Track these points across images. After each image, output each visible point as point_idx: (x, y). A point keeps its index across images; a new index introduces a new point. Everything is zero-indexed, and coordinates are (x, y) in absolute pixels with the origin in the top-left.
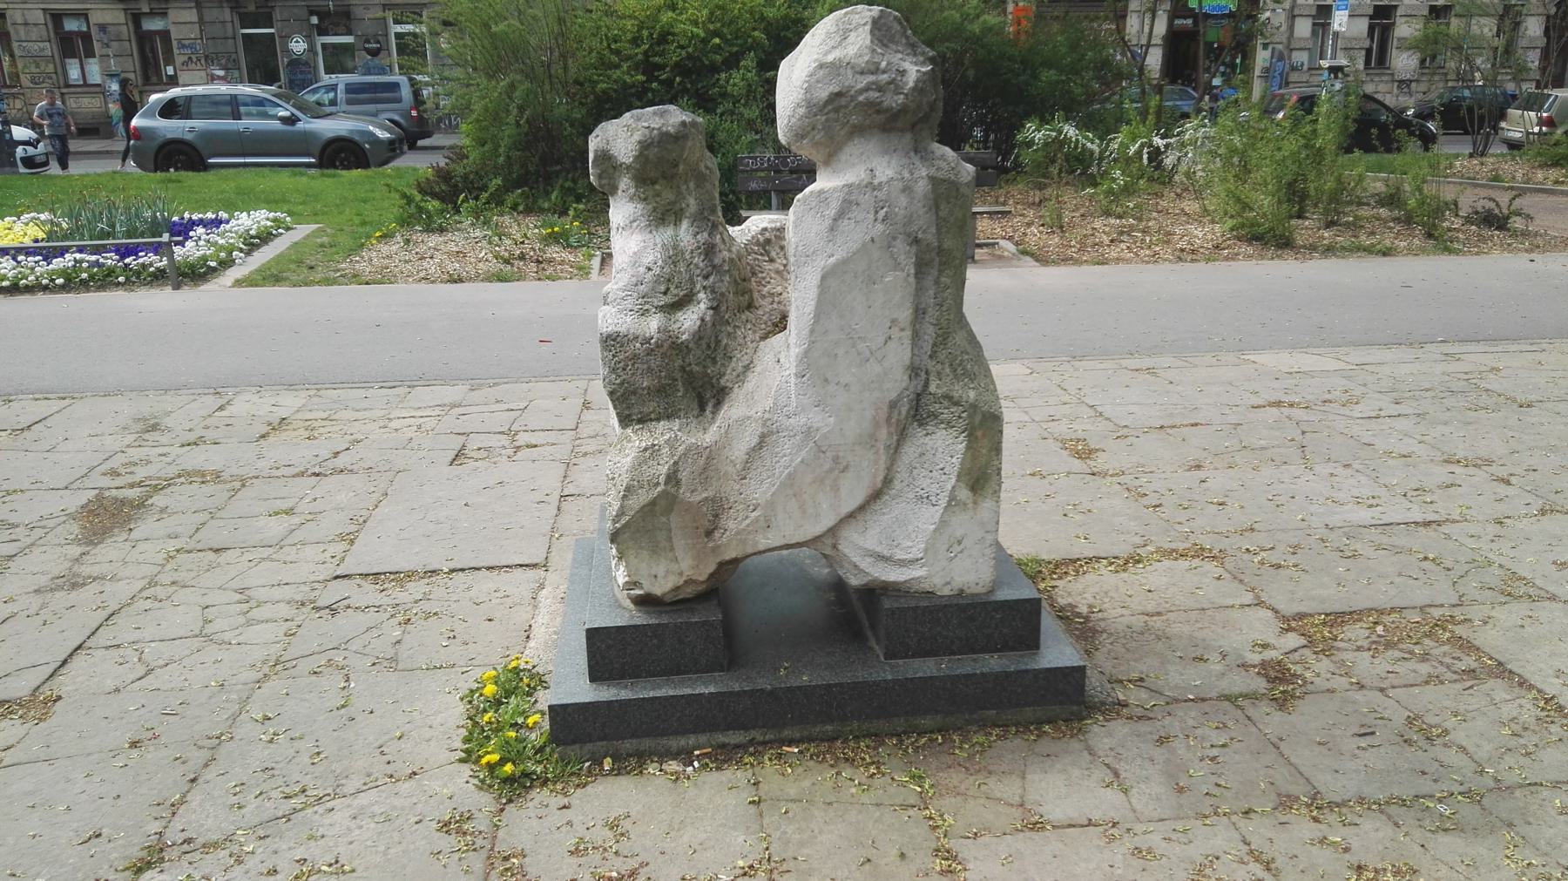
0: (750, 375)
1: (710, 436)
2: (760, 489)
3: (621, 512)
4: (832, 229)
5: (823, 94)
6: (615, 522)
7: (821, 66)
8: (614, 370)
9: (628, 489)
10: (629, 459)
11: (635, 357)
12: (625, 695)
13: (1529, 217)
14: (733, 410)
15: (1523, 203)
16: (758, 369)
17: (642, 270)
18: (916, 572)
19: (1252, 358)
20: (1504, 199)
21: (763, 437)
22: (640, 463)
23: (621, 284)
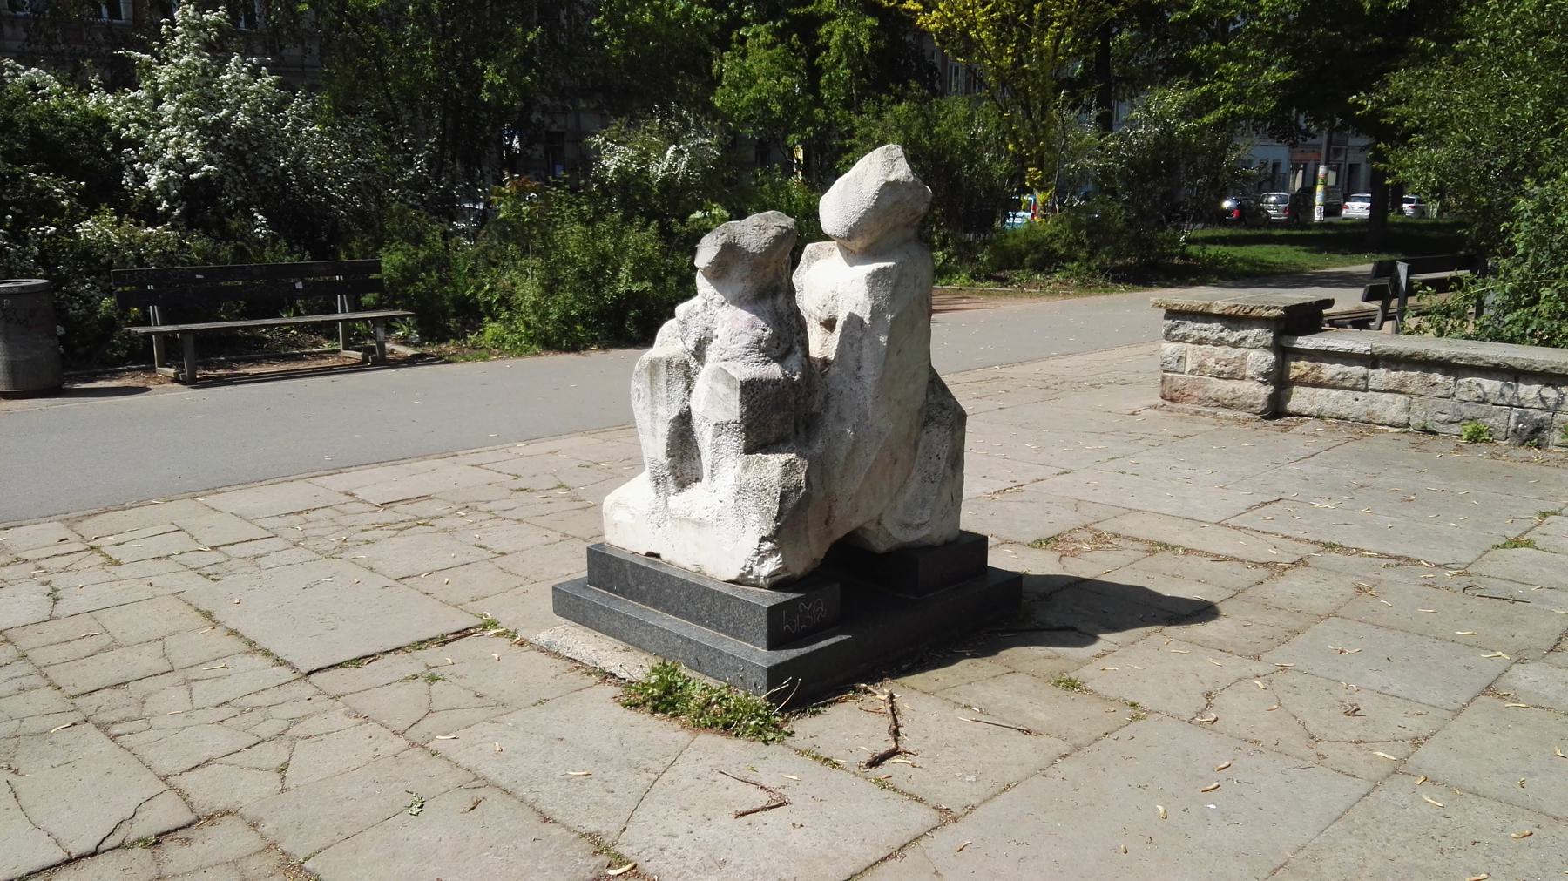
3: (780, 513)
9: (783, 495)
18: (924, 532)
22: (785, 474)
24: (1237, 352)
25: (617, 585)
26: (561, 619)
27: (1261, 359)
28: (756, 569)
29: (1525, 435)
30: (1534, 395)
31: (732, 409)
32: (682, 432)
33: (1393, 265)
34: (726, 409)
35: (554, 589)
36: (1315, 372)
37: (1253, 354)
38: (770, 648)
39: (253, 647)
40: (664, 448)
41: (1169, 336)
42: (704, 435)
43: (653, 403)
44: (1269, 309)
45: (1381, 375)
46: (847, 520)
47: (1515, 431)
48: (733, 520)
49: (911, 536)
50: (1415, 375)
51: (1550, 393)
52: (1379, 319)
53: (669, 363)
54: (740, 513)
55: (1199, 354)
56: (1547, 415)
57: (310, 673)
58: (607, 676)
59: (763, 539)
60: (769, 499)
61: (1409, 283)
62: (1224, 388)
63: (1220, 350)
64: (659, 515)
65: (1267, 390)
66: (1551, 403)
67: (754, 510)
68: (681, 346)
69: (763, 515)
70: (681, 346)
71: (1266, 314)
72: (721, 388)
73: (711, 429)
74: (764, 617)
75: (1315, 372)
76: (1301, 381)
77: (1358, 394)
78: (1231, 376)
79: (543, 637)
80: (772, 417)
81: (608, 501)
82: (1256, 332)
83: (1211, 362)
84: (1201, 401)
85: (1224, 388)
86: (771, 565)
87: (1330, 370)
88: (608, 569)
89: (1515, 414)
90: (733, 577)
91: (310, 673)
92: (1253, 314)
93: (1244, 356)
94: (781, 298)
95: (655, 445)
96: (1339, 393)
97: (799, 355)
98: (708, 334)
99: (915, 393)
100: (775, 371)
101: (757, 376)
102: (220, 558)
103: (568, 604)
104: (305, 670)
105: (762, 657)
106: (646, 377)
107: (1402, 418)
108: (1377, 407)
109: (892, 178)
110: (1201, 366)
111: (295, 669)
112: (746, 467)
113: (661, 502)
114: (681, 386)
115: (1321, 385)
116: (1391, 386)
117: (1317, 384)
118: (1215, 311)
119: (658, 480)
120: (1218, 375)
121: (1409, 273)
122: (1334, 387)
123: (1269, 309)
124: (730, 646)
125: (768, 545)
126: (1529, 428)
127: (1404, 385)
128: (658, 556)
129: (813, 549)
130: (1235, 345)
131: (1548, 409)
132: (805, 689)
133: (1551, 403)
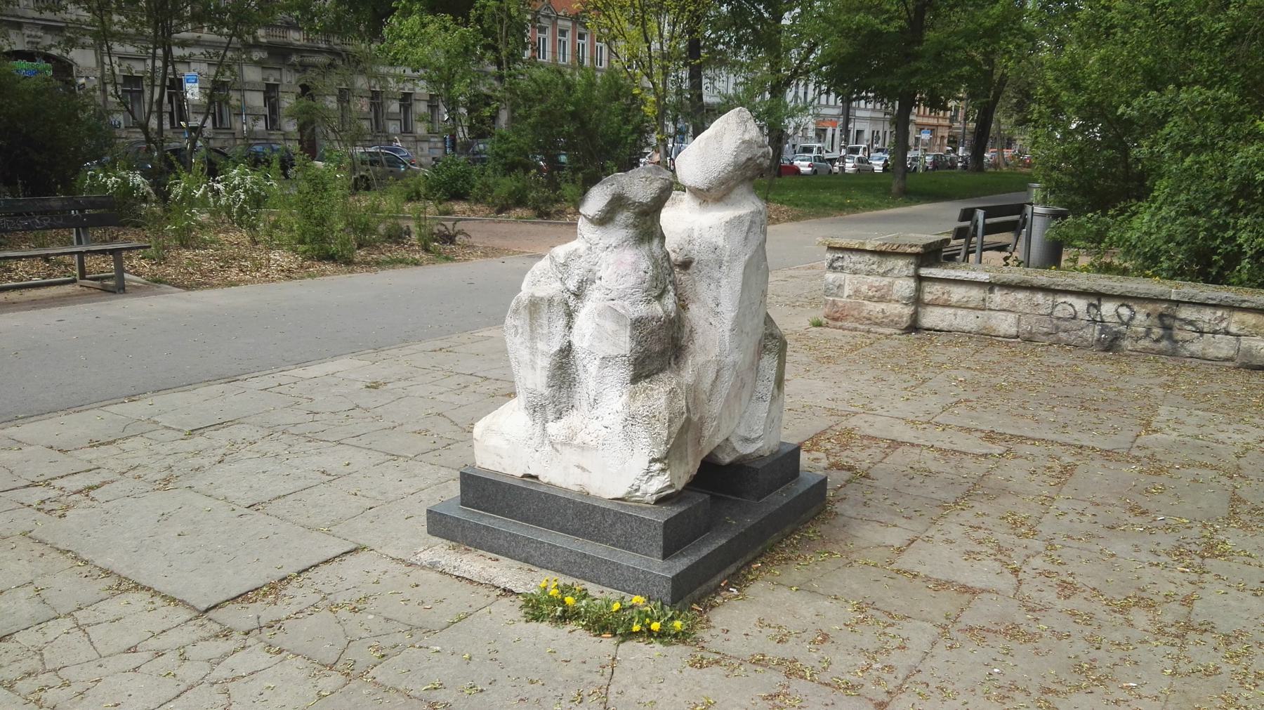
0: (696, 336)
1: (688, 376)
2: (716, 407)
3: (669, 437)
4: (746, 238)
5: (743, 158)
6: (666, 444)
7: (743, 142)
8: (639, 343)
9: (670, 421)
10: (662, 400)
11: (653, 331)
12: (705, 551)
13: (468, 235)
14: (698, 359)
15: (459, 226)
16: (700, 331)
17: (642, 273)
18: (759, 444)
19: (486, 333)
20: (449, 225)
21: (718, 371)
22: (671, 401)
23: (629, 285)
24: (886, 281)
25: (495, 508)
26: (436, 539)
27: (905, 286)
28: (643, 487)
29: (1107, 343)
30: (1112, 312)
31: (624, 344)
32: (564, 367)
33: (973, 211)
34: (615, 344)
35: (429, 511)
36: (946, 296)
37: (899, 282)
38: (665, 557)
39: (124, 585)
40: (545, 380)
41: (832, 267)
42: (589, 371)
43: (532, 339)
44: (911, 246)
45: (998, 297)
46: (712, 438)
47: (1099, 340)
48: (621, 444)
49: (749, 449)
50: (1021, 295)
51: (1125, 312)
52: (963, 254)
53: (550, 301)
54: (628, 437)
55: (854, 282)
56: (1123, 328)
57: (207, 610)
58: (507, 592)
59: (654, 460)
60: (658, 425)
61: (985, 226)
62: (876, 308)
63: (870, 279)
64: (537, 440)
65: (908, 311)
66: (1125, 318)
67: (644, 434)
68: (558, 286)
69: (654, 439)
70: (558, 286)
71: (909, 250)
72: (609, 325)
73: (597, 362)
74: (660, 531)
75: (946, 296)
76: (933, 304)
77: (979, 313)
78: (881, 299)
79: (425, 557)
80: (659, 348)
81: (478, 429)
82: (901, 263)
83: (864, 288)
84: (857, 320)
85: (876, 308)
86: (658, 484)
87: (958, 293)
88: (483, 491)
89: (1098, 327)
90: (620, 496)
91: (207, 610)
92: (899, 250)
93: (891, 285)
94: (656, 242)
95: (533, 376)
96: (965, 312)
97: (672, 294)
98: (590, 275)
99: (755, 328)
100: (657, 309)
101: (644, 314)
102: (53, 493)
103: (439, 525)
104: (204, 606)
105: (664, 570)
106: (524, 314)
107: (1013, 331)
108: (993, 322)
109: (747, 137)
110: (857, 291)
111: (193, 608)
112: (633, 396)
113: (538, 428)
114: (562, 322)
115: (949, 306)
116: (1005, 306)
117: (946, 305)
118: (868, 248)
119: (536, 409)
120: (870, 299)
121: (986, 217)
122: (959, 307)
123: (911, 246)
124: (628, 559)
125: (658, 466)
126: (1110, 338)
127: (1014, 306)
128: (536, 477)
129: (690, 467)
130: (884, 274)
131: (1123, 323)
132: (692, 593)
133: (1125, 318)
